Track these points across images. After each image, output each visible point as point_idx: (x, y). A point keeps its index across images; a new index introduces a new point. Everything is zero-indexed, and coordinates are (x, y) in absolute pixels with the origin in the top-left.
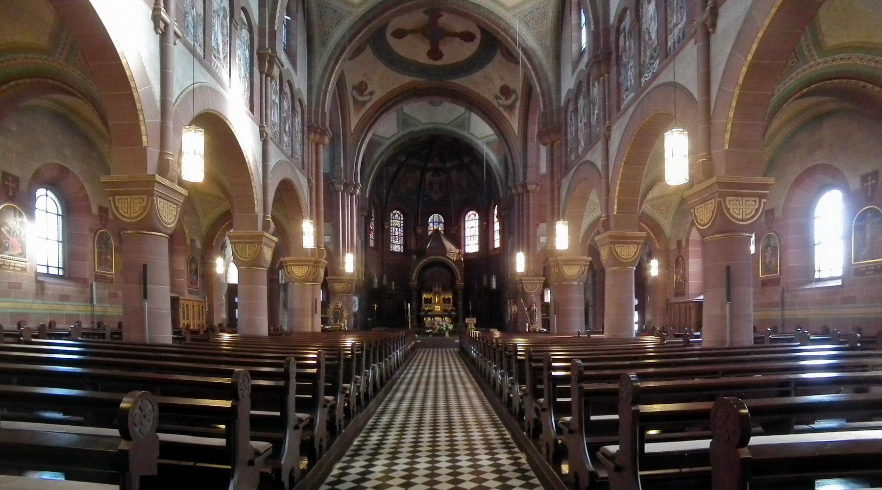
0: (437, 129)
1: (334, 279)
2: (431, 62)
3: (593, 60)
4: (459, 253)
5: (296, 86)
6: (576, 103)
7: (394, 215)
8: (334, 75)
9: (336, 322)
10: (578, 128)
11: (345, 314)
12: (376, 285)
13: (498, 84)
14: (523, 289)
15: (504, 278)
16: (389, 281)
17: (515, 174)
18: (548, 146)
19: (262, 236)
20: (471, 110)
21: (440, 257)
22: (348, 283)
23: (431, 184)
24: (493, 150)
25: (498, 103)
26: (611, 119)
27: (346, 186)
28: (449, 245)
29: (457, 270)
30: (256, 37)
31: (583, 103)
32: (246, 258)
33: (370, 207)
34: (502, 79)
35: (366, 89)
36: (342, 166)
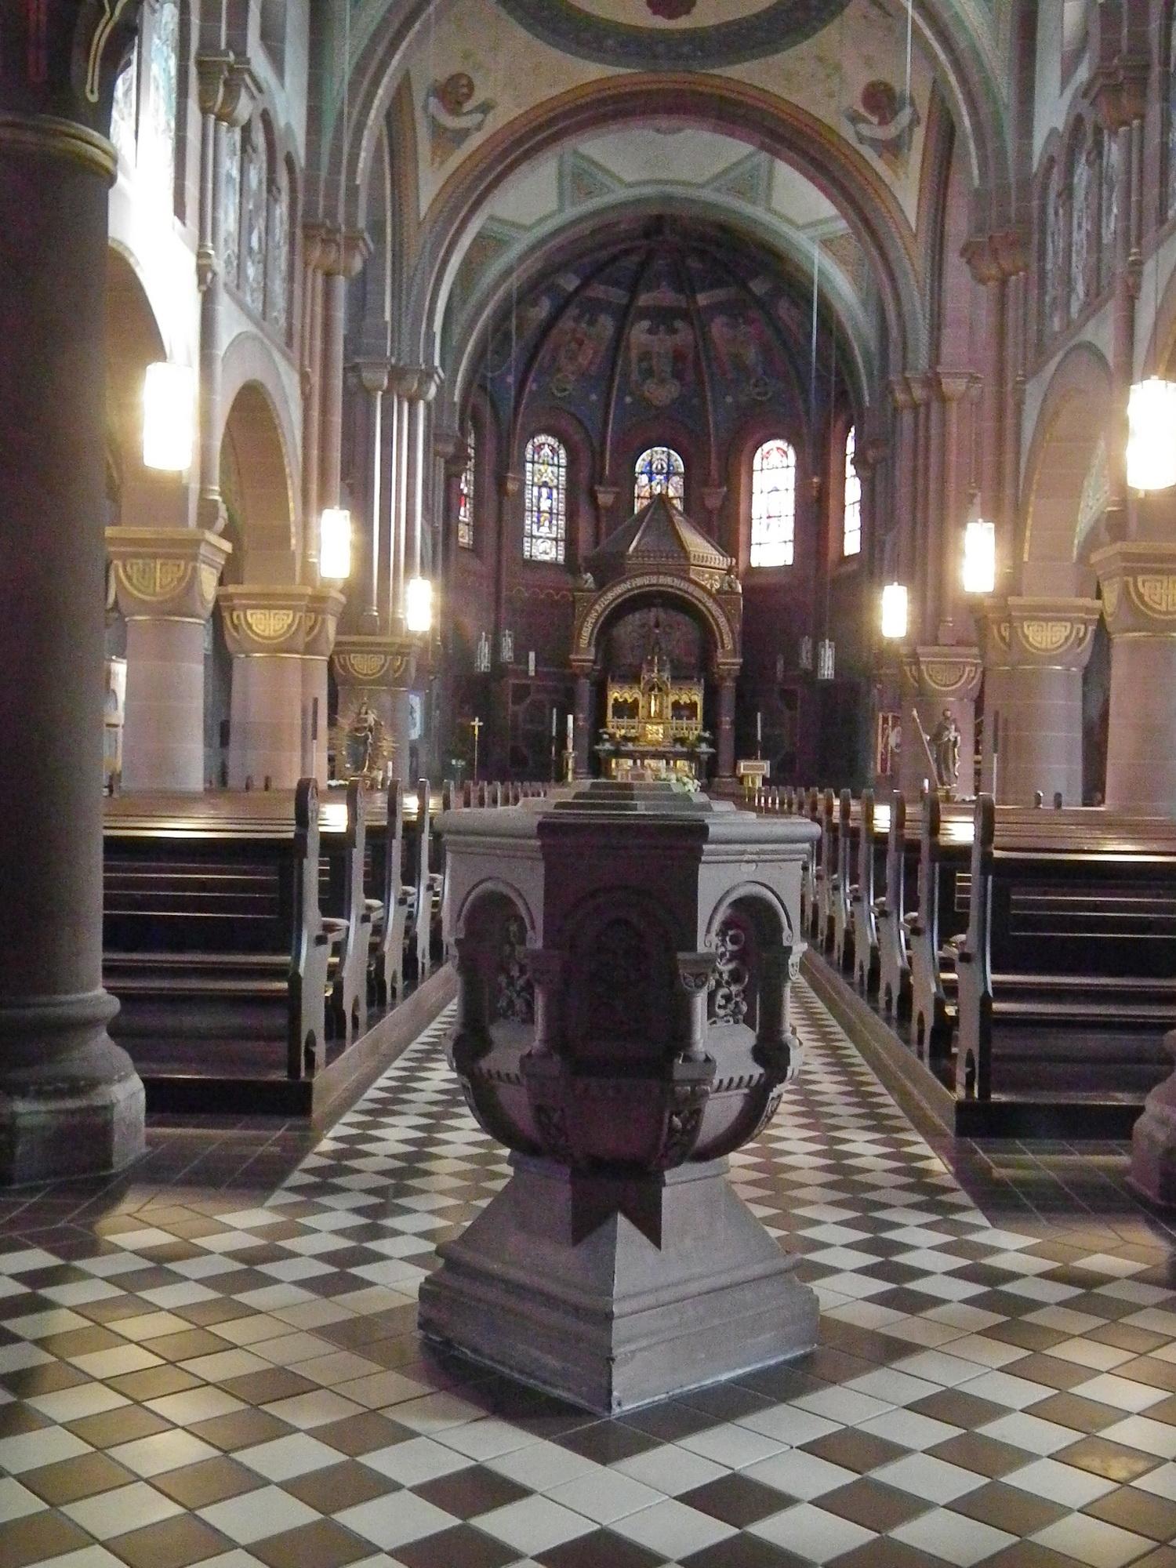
0: (668, 199)
1: (354, 644)
2: (661, 23)
3: (1100, 81)
4: (729, 571)
5: (281, 121)
6: (1069, 172)
7: (540, 447)
8: (385, 80)
9: (358, 767)
10: (1070, 245)
11: (387, 744)
12: (483, 664)
13: (859, 79)
14: (920, 680)
15: (869, 640)
16: (520, 657)
17: (905, 348)
18: (991, 284)
19: (197, 543)
20: (775, 153)
21: (669, 580)
22: (398, 653)
23: (646, 356)
24: (842, 261)
25: (857, 133)
26: (1143, 242)
27: (398, 375)
28: (697, 544)
29: (722, 620)
30: (195, 20)
31: (1085, 177)
32: (154, 594)
33: (462, 428)
34: (869, 62)
35: (469, 96)
36: (388, 316)
